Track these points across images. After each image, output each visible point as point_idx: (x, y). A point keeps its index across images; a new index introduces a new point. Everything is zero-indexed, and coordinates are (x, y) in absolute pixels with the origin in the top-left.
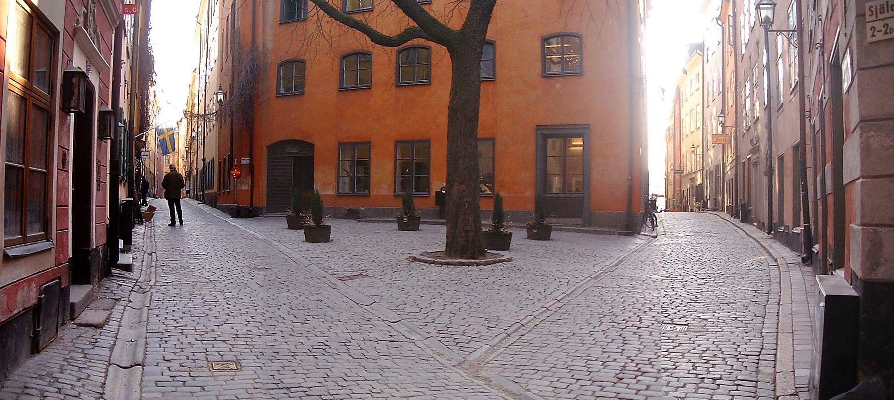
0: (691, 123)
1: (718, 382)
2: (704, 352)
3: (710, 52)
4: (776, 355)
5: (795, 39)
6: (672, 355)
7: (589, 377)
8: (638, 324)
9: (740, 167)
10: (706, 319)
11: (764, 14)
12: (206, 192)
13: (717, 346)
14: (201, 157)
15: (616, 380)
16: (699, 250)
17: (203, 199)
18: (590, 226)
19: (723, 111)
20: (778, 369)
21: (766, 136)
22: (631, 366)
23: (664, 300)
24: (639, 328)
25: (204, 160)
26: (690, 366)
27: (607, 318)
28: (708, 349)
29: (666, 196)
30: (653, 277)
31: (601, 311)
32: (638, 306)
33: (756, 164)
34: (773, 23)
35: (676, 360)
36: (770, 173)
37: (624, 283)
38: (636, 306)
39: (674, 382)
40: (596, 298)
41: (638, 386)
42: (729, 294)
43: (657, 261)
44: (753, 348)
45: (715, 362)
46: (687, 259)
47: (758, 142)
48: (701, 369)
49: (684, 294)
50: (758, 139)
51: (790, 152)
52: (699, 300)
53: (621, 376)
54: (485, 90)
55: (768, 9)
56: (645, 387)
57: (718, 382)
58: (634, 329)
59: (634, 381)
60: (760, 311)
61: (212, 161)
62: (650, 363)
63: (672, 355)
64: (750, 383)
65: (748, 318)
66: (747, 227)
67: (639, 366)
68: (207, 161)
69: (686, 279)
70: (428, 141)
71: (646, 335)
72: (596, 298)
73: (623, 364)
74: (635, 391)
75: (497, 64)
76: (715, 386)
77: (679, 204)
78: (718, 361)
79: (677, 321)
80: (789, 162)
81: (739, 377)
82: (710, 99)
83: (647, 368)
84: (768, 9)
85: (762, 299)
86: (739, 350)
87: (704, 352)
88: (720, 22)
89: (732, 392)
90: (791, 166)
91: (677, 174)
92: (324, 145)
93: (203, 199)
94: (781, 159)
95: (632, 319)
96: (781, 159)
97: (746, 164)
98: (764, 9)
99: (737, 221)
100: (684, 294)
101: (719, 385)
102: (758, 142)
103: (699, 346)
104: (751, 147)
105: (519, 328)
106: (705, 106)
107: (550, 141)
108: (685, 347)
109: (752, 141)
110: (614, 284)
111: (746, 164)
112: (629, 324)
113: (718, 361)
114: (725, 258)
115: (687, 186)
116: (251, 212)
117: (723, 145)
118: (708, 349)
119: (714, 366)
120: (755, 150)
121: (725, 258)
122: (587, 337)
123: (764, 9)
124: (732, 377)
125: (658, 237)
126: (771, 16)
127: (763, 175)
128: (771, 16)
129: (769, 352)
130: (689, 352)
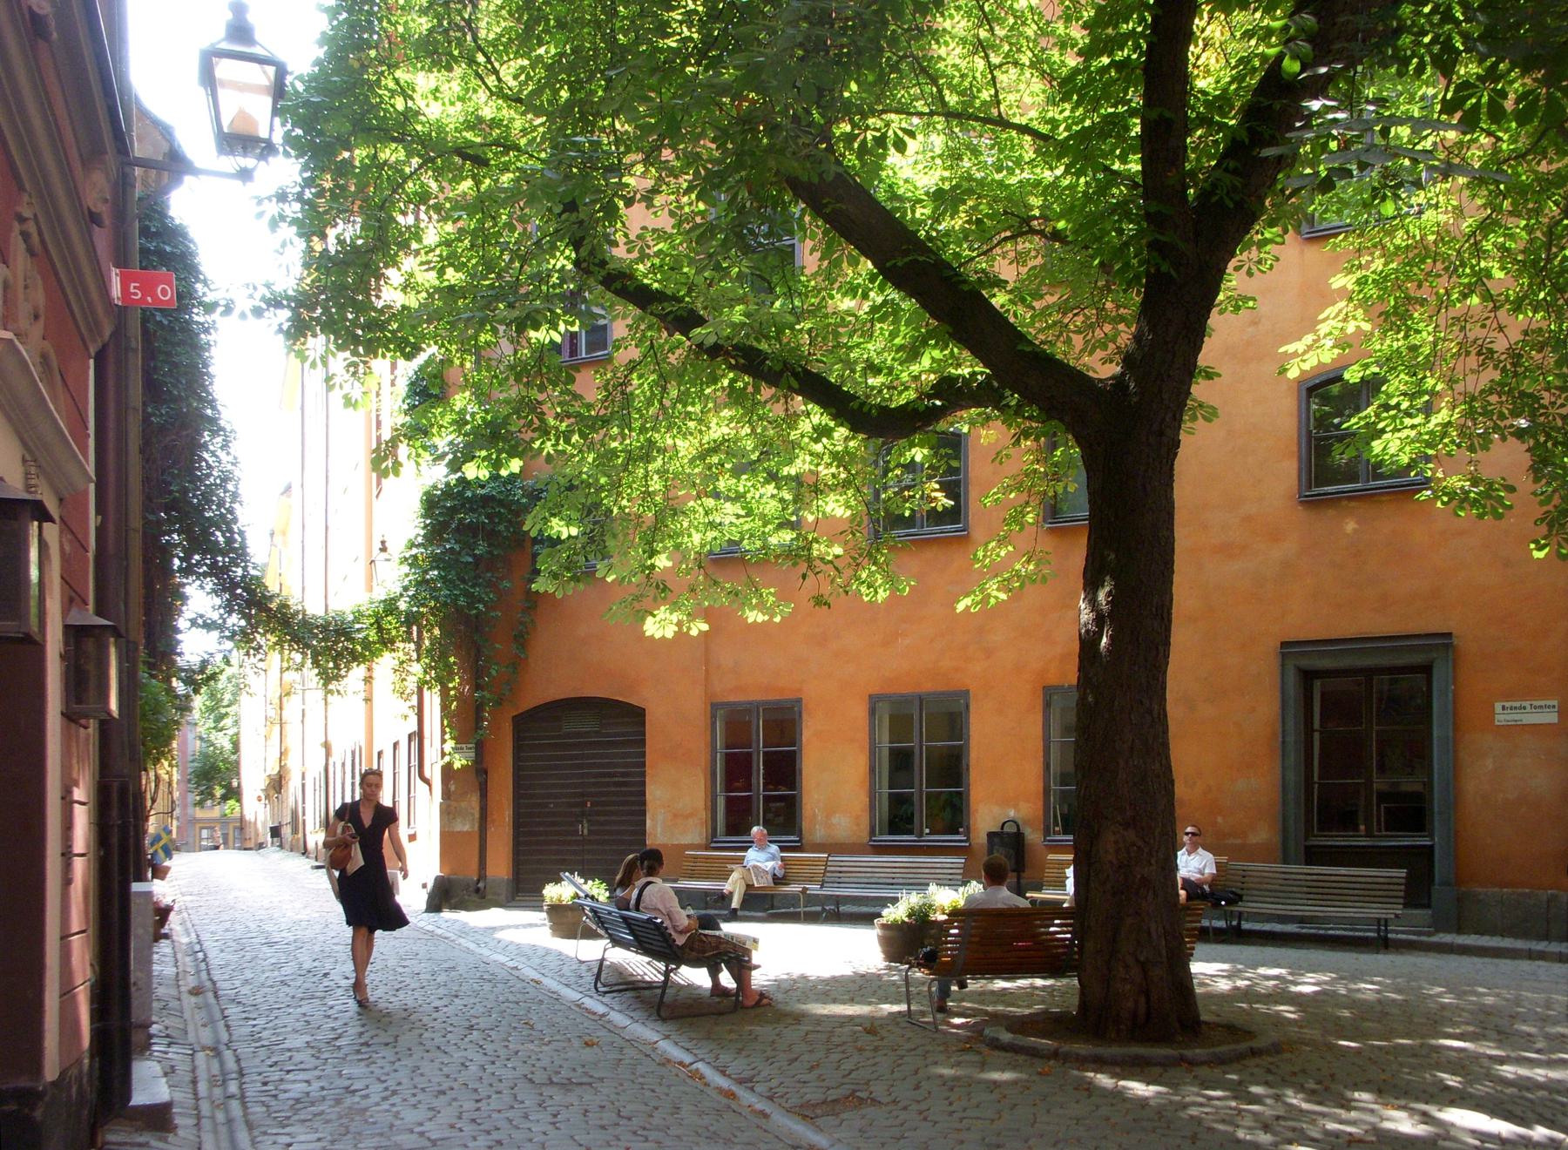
18: (1459, 931)
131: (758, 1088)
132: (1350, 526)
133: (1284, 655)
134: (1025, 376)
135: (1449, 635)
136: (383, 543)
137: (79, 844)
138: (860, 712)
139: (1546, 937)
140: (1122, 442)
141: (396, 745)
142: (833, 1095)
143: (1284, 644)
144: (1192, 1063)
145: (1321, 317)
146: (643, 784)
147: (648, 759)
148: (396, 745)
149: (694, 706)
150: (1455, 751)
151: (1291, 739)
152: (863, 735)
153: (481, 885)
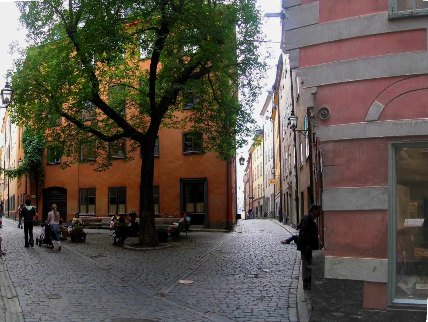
0: (258, 182)
1: (271, 298)
2: (265, 286)
3: (267, 135)
4: (297, 286)
5: (307, 134)
6: (251, 288)
7: (214, 297)
8: (234, 273)
9: (283, 196)
10: (266, 272)
11: (292, 122)
12: (10, 212)
13: (271, 283)
14: (6, 193)
15: (225, 297)
16: (262, 239)
17: (8, 216)
18: (208, 228)
19: (274, 168)
20: (298, 292)
21: (295, 180)
22: (232, 291)
23: (246, 263)
24: (234, 275)
25: (8, 195)
26: (259, 292)
27: (219, 272)
28: (267, 285)
29: (245, 211)
30: (240, 252)
31: (216, 268)
32: (233, 265)
33: (291, 195)
34: (296, 127)
35: (253, 290)
36: (297, 200)
37: (226, 255)
38: (233, 265)
39: (252, 298)
40: (213, 263)
41: (235, 299)
42: (277, 260)
43: (242, 245)
44: (288, 284)
45: (270, 290)
46: (257, 244)
47: (291, 184)
48: (264, 293)
49: (255, 260)
50: (291, 182)
51: (306, 190)
52: (262, 263)
53: (227, 295)
54: (156, 161)
55: (294, 120)
56: (238, 299)
57: (271, 298)
58: (232, 276)
59: (233, 297)
60: (291, 267)
61: (14, 195)
62: (240, 289)
63: (251, 288)
64: (286, 298)
65: (285, 271)
66: (286, 227)
67: (235, 291)
68: (10, 196)
69: (256, 253)
70: (126, 186)
71: (237, 277)
72: (213, 263)
73: (228, 291)
74: (234, 301)
75: (160, 147)
76: (270, 300)
77: (251, 215)
78: (271, 290)
79: (252, 273)
80: (306, 195)
81: (281, 296)
82: (268, 160)
83: (239, 291)
84: (294, 120)
85: (292, 262)
86: (281, 285)
87: (265, 286)
88: (272, 120)
89: (278, 302)
90: (307, 197)
91: (251, 199)
92: (72, 189)
93: (8, 216)
94: (302, 194)
95: (231, 271)
96: (302, 194)
97: (286, 195)
98: (292, 120)
99: (282, 224)
100: (255, 260)
101: (272, 299)
102: (291, 184)
103: (263, 283)
104: (288, 186)
105: (199, 263)
106: (265, 163)
107: (187, 186)
108: (257, 284)
109: (288, 183)
110: (222, 256)
111: (286, 195)
112: (230, 274)
113: (271, 290)
114: (276, 243)
115: (256, 204)
116: (36, 223)
117: (274, 185)
118: (267, 285)
119: (269, 291)
120: (290, 188)
121: (276, 243)
122: (211, 281)
123: (292, 120)
124: (278, 296)
125: (242, 233)
126: (295, 124)
127: (294, 200)
128: (295, 124)
129: (295, 285)
130: (259, 286)
131: (84, 254)
132: (191, 159)
133: (181, 181)
134: (129, 132)
135: (206, 178)
136: (20, 158)
137: (134, 248)
138: (106, 190)
139: (221, 228)
140: (148, 142)
141: (21, 195)
142: (97, 255)
143: (181, 179)
144: (156, 250)
145: (123, 138)
146: (66, 203)
147: (67, 198)
148: (21, 195)
149: (76, 188)
150: (208, 198)
151: (182, 196)
152: (107, 194)
153: (37, 221)
